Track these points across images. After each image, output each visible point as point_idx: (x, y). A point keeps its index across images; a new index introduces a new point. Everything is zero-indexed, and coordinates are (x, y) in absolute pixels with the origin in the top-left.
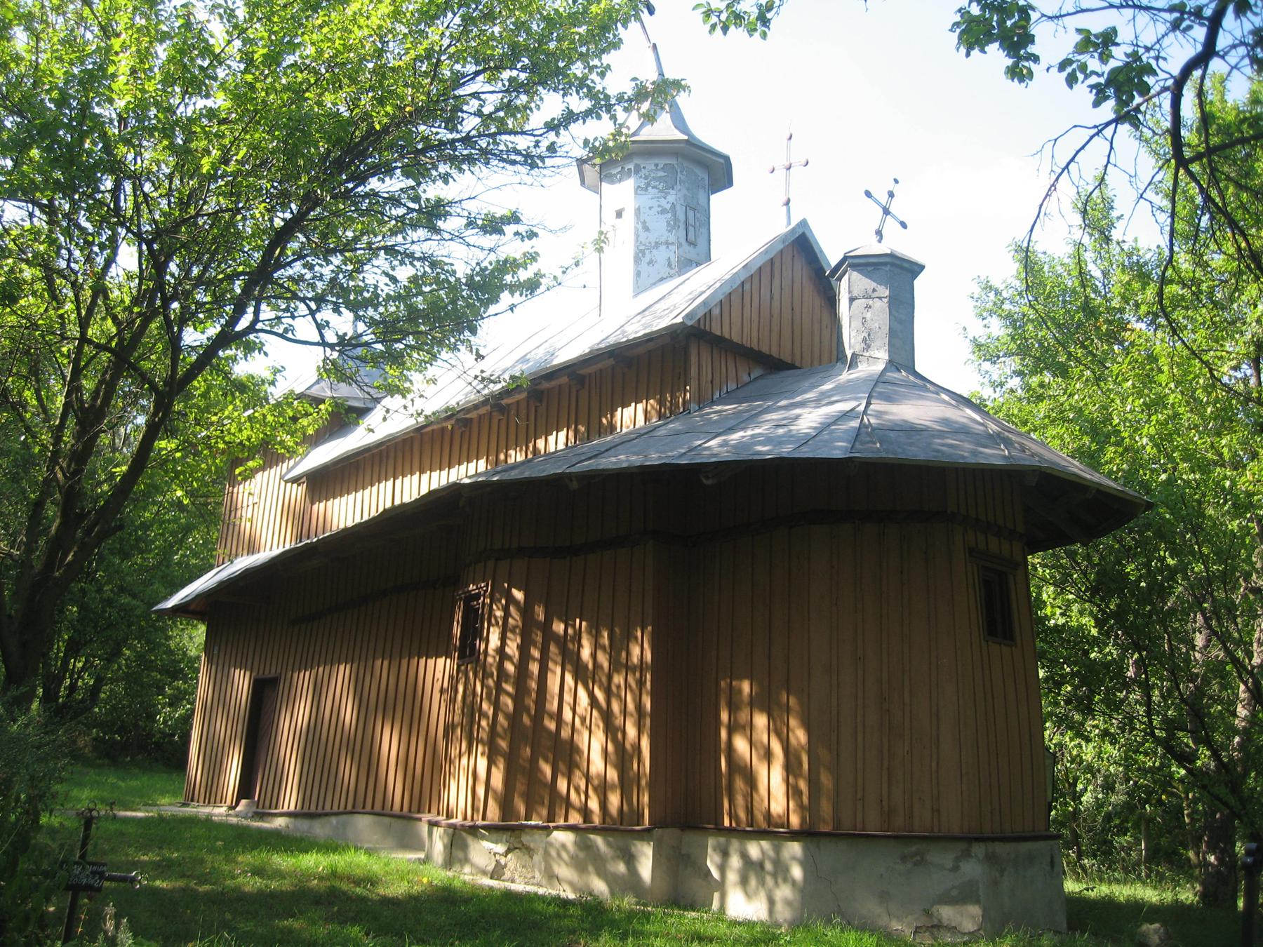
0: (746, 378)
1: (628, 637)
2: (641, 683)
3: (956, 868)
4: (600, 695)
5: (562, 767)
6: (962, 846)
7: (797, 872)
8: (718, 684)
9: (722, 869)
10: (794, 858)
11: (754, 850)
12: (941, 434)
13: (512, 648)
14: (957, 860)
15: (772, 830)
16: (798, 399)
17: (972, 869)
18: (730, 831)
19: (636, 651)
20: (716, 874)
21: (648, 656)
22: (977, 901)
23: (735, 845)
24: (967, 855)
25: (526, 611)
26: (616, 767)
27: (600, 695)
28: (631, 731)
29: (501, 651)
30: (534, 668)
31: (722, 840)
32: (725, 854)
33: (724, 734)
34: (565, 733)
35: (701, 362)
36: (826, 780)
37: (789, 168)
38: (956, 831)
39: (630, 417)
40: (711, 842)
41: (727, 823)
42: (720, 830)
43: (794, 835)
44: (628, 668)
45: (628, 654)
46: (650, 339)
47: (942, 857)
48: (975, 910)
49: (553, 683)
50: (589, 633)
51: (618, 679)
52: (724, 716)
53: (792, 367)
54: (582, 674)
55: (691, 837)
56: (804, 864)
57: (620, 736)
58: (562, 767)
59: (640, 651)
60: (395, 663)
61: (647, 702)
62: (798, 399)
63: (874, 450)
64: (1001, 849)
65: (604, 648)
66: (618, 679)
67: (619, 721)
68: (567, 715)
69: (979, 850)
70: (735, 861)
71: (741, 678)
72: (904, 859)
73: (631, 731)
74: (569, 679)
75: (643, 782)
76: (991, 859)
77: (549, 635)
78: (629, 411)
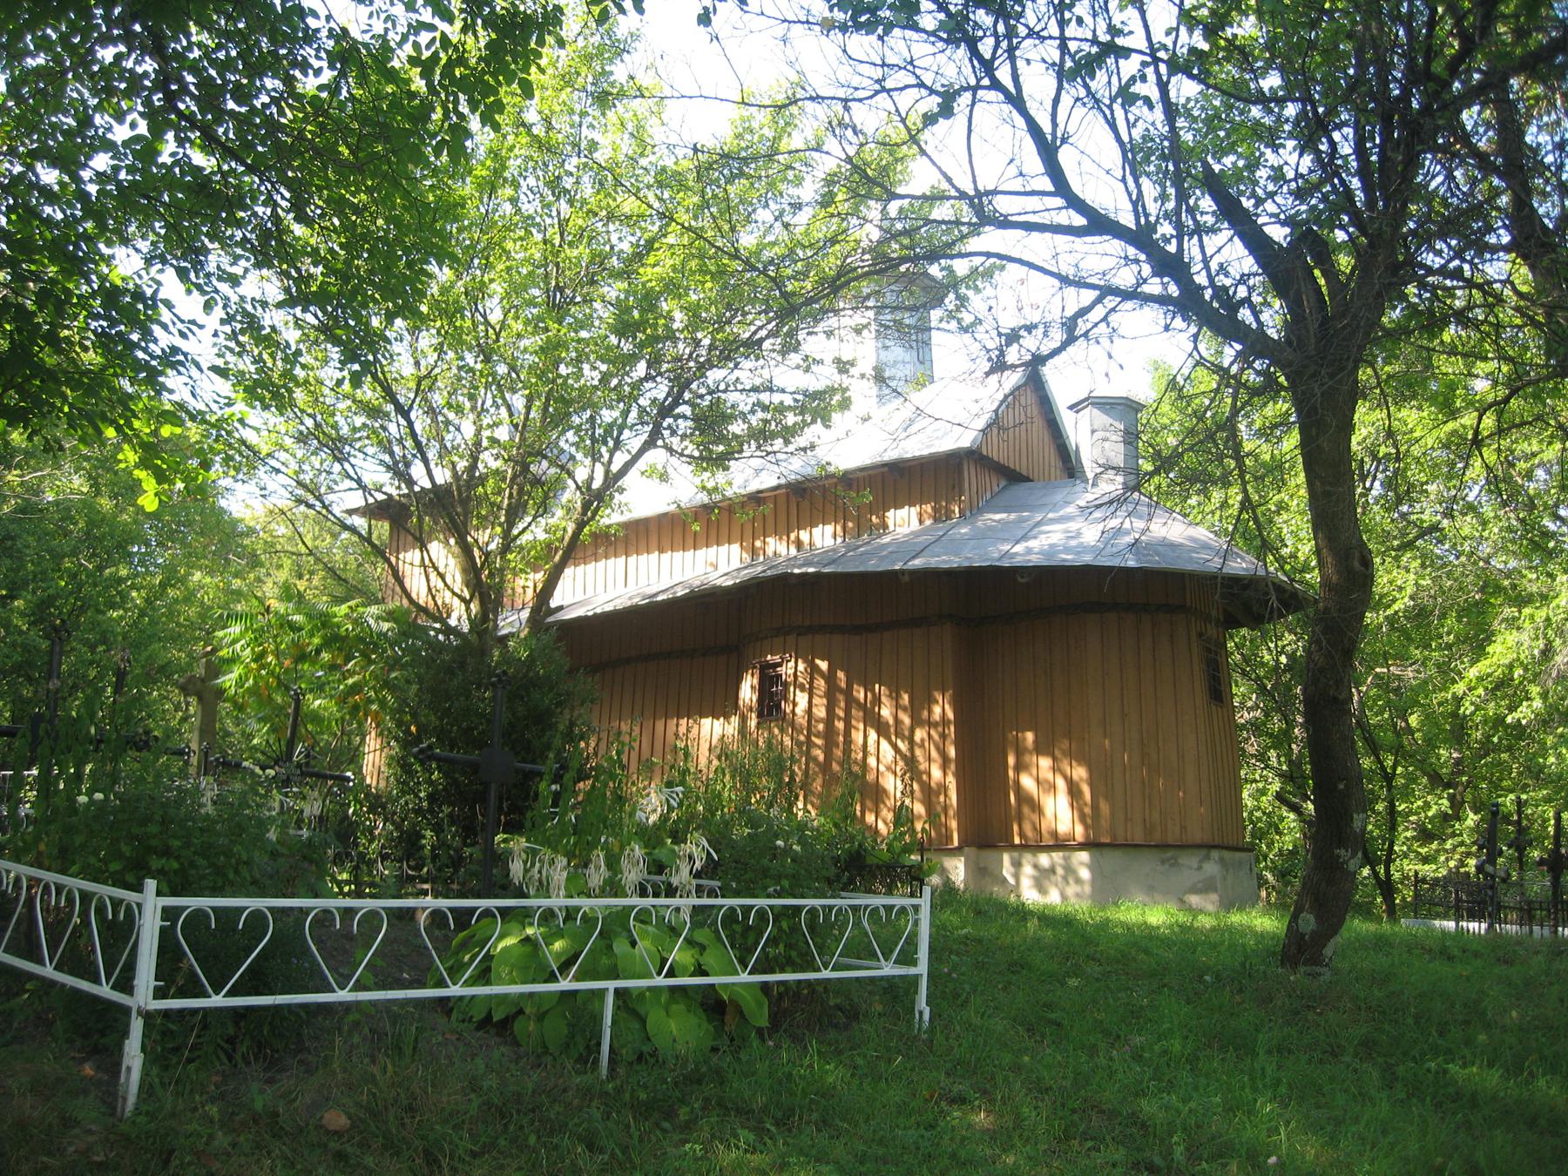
0: (996, 489)
1: (931, 701)
2: (943, 736)
3: (1200, 868)
4: (902, 746)
5: (869, 803)
6: (1204, 852)
7: (1085, 874)
8: (1004, 737)
9: (1017, 876)
10: (1082, 863)
11: (1044, 859)
12: (1194, 550)
13: (820, 712)
14: (1201, 861)
15: (1060, 844)
16: (1062, 513)
17: (1211, 868)
18: (1025, 847)
19: (937, 710)
20: (1012, 881)
21: (950, 715)
22: (1215, 890)
23: (1027, 858)
24: (1207, 858)
25: (830, 678)
26: (923, 802)
27: (902, 746)
28: (936, 773)
29: (809, 711)
30: (840, 725)
31: (1016, 854)
32: (1017, 865)
33: (1011, 773)
34: (871, 777)
35: (970, 474)
36: (1104, 807)
37: (1110, 357)
38: (1198, 841)
39: (904, 521)
40: (1006, 858)
41: (1017, 841)
42: (1013, 847)
43: (1082, 846)
44: (930, 724)
45: (930, 712)
46: (921, 458)
47: (1190, 860)
48: (1214, 897)
49: (858, 737)
50: (890, 696)
51: (919, 734)
52: (1011, 760)
53: (1028, 479)
54: (882, 729)
55: (989, 855)
56: (1091, 867)
57: (925, 777)
58: (869, 803)
59: (942, 708)
60: (648, 724)
61: (952, 752)
62: (1062, 513)
63: (1155, 562)
64: (1227, 854)
65: (905, 709)
66: (919, 734)
67: (923, 766)
68: (872, 761)
69: (1215, 854)
70: (1028, 870)
71: (1025, 730)
72: (1163, 862)
73: (936, 773)
74: (873, 735)
75: (951, 813)
76: (1222, 860)
77: (851, 701)
78: (903, 513)
